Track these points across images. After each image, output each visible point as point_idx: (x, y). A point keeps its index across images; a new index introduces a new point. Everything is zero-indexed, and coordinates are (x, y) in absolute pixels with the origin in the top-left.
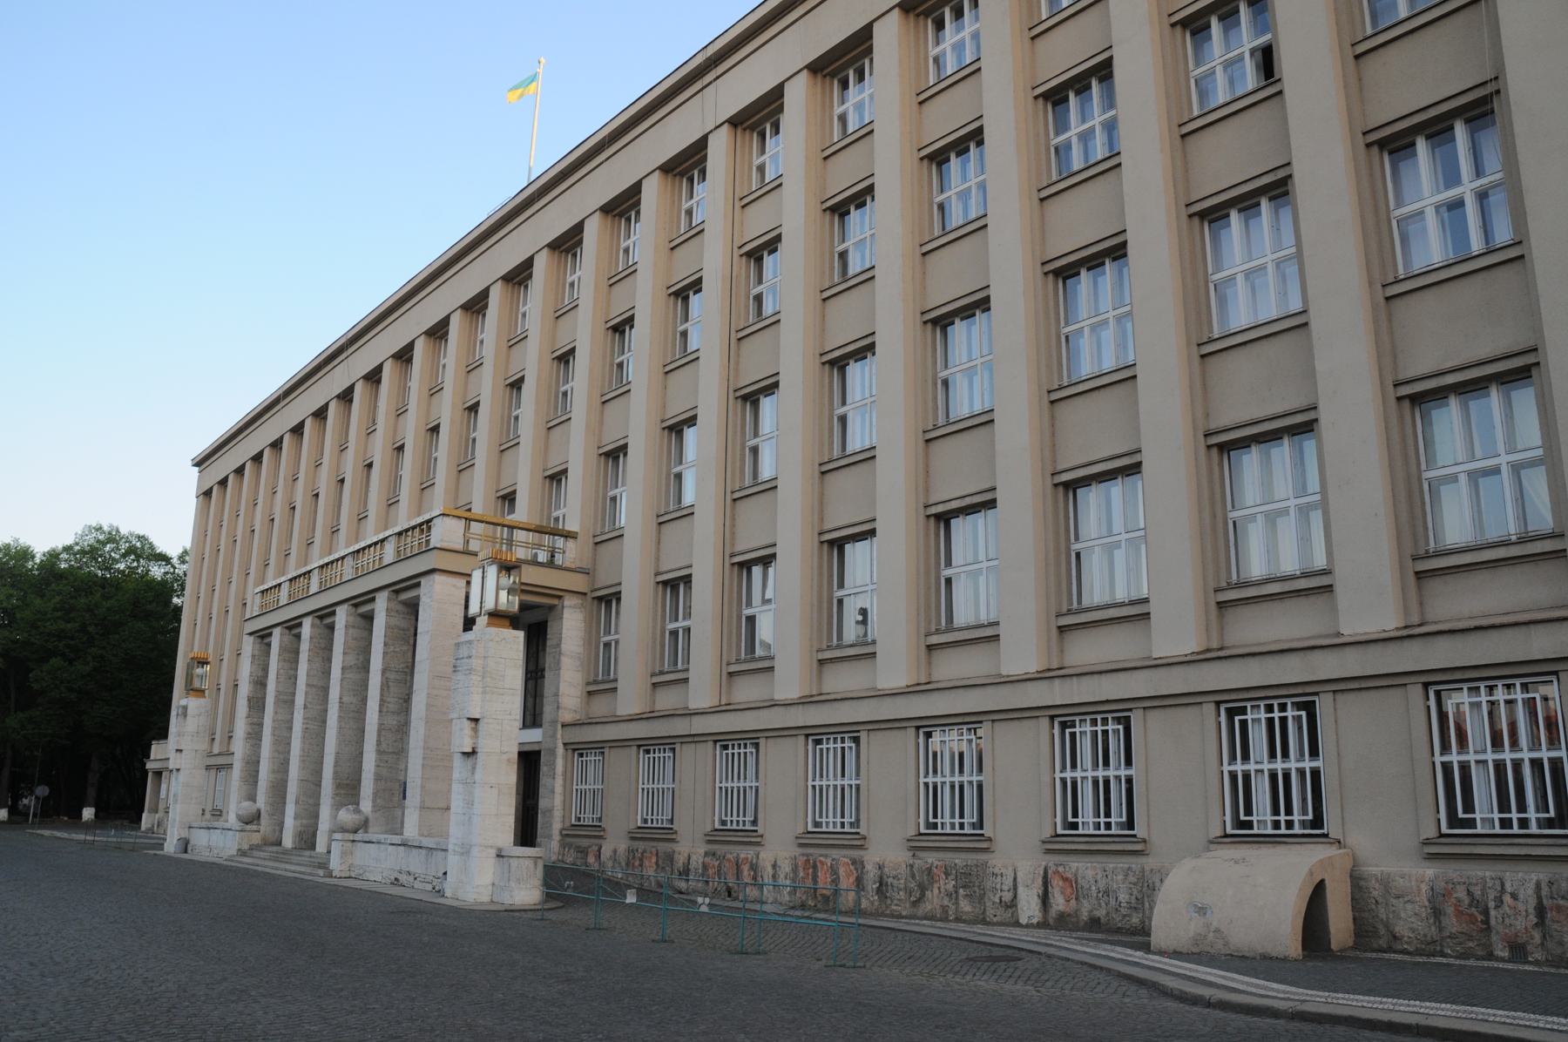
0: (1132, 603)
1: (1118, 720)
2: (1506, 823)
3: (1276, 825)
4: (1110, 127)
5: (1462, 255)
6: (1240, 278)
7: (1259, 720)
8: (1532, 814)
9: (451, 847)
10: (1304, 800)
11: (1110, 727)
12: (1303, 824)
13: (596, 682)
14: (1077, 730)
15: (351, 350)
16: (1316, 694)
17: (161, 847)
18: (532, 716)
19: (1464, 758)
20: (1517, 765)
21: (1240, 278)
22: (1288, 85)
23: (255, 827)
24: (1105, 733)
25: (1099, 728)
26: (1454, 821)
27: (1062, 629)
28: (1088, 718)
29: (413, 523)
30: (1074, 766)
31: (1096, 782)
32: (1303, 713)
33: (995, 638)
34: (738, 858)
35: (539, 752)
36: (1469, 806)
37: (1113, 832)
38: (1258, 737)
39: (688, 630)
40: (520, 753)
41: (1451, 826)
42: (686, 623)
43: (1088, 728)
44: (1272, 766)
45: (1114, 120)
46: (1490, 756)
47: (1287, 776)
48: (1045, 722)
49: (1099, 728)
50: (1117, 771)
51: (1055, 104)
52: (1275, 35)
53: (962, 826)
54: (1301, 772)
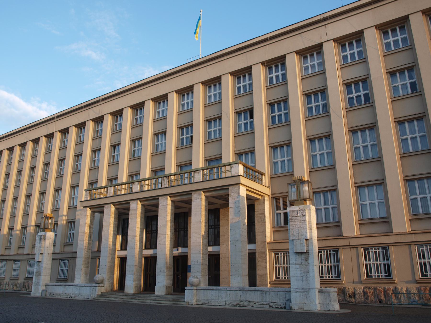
2: (378, 276)
3: (329, 277)
8: (334, 275)
9: (292, 290)
13: (7, 246)
15: (102, 102)
17: (30, 294)
18: (251, 239)
23: (102, 285)
27: (64, 245)
34: (385, 288)
38: (281, 260)
39: (73, 233)
40: (249, 253)
41: (422, 276)
42: (73, 232)
51: (181, 129)
52: (328, 101)
54: (335, 266)
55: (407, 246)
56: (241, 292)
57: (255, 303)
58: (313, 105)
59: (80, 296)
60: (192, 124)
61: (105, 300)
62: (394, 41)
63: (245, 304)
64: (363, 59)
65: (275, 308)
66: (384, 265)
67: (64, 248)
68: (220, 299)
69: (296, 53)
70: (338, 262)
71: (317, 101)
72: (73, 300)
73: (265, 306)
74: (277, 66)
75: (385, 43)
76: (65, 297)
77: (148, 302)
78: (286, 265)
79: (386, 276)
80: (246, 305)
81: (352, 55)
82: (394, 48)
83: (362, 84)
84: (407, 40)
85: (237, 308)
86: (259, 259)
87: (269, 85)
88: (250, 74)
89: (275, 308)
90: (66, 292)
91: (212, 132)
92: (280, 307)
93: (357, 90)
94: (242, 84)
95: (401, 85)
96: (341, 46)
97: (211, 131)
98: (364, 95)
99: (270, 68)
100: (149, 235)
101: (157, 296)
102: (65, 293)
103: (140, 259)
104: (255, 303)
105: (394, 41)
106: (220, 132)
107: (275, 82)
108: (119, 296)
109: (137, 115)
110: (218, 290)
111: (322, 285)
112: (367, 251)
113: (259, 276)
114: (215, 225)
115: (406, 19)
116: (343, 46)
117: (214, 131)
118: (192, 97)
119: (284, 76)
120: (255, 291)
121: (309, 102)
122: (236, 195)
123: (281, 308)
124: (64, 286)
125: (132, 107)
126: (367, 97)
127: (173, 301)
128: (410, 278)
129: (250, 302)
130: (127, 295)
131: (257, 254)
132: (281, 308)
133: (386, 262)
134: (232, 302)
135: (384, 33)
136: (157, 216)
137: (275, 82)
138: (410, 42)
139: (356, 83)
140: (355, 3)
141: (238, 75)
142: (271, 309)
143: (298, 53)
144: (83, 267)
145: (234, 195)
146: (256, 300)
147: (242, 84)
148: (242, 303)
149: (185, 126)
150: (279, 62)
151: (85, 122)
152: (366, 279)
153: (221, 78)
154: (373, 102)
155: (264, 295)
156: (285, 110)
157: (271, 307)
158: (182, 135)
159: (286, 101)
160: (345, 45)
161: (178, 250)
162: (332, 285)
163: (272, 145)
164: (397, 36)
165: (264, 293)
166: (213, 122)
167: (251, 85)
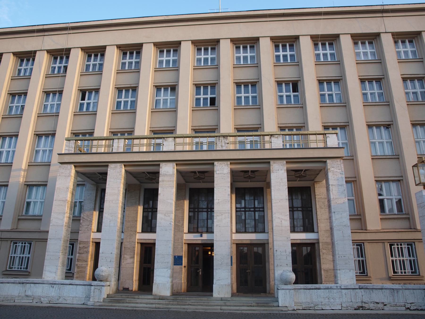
0: (38, 216)
1: (29, 243)
3: (402, 273)
4: (59, 105)
5: (6, 162)
6: (41, 151)
7: (406, 247)
11: (26, 245)
12: (24, 268)
14: (18, 245)
15: (71, 32)
20: (396, 261)
21: (41, 151)
24: (25, 246)
25: (23, 245)
28: (21, 242)
30: (15, 253)
31: (20, 257)
33: (41, 219)
37: (22, 270)
43: (20, 244)
45: (60, 104)
46: (409, 258)
48: (9, 242)
49: (23, 245)
50: (26, 255)
51: (47, 94)
55: (381, 243)
56: (362, 290)
57: (385, 305)
58: (123, 100)
59: (60, 301)
60: (63, 91)
61: (127, 306)
62: (204, 59)
63: (372, 306)
64: (176, 68)
65: (414, 310)
66: (400, 261)
67: (18, 224)
68: (332, 300)
69: (117, 47)
70: (362, 256)
71: (205, 93)
72: (45, 307)
73: (399, 308)
74: (96, 56)
75: (197, 59)
76: (26, 302)
77: (200, 308)
78: (412, 258)
79: (361, 273)
80: (373, 308)
81: (168, 62)
82: (173, 66)
83: (203, 89)
84: (208, 61)
85: (360, 312)
86: (324, 251)
87: (120, 69)
88: (103, 55)
89: (414, 310)
90: (27, 294)
91: (14, 107)
92: (420, 308)
93: (126, 97)
94: (58, 65)
95: (170, 99)
96: (123, 54)
97: (48, 105)
98: (211, 98)
99: (90, 56)
100: (192, 214)
101: (217, 299)
102: (27, 296)
103: (228, 244)
104: (385, 305)
105: (166, 60)
106: (58, 107)
107: (127, 68)
108: (148, 301)
109: (21, 65)
110: (328, 289)
111: (358, 282)
112: (393, 247)
113: (324, 270)
114: (207, 208)
115: (217, 41)
116: (125, 54)
117: (16, 106)
118: (33, 65)
119: (138, 64)
120: (382, 289)
121: (120, 96)
122: (338, 171)
123: (422, 310)
124: (23, 283)
125: (120, 47)
126: (213, 101)
127: (258, 306)
128: (384, 276)
129: (378, 303)
130: (162, 298)
131: (321, 244)
132: (422, 310)
133: (361, 259)
134: (351, 304)
135: (236, 47)
136: (213, 189)
137: (127, 68)
138: (217, 63)
139: (206, 86)
140: (263, 11)
141: (131, 49)
142: (408, 312)
143: (156, 45)
144: (61, 254)
145: (335, 170)
146: (386, 301)
147: (58, 65)
148: (366, 305)
149: (88, 90)
150: (135, 50)
151: (35, 52)
152: (393, 275)
153: (106, 48)
154: (219, 106)
155: (396, 295)
156: (88, 100)
157: (408, 308)
158: (281, 91)
159: (135, 89)
160: (126, 53)
161: (201, 236)
162: (413, 282)
163: (194, 128)
164: (208, 55)
165: (396, 291)
166: (51, 95)
167: (101, 65)
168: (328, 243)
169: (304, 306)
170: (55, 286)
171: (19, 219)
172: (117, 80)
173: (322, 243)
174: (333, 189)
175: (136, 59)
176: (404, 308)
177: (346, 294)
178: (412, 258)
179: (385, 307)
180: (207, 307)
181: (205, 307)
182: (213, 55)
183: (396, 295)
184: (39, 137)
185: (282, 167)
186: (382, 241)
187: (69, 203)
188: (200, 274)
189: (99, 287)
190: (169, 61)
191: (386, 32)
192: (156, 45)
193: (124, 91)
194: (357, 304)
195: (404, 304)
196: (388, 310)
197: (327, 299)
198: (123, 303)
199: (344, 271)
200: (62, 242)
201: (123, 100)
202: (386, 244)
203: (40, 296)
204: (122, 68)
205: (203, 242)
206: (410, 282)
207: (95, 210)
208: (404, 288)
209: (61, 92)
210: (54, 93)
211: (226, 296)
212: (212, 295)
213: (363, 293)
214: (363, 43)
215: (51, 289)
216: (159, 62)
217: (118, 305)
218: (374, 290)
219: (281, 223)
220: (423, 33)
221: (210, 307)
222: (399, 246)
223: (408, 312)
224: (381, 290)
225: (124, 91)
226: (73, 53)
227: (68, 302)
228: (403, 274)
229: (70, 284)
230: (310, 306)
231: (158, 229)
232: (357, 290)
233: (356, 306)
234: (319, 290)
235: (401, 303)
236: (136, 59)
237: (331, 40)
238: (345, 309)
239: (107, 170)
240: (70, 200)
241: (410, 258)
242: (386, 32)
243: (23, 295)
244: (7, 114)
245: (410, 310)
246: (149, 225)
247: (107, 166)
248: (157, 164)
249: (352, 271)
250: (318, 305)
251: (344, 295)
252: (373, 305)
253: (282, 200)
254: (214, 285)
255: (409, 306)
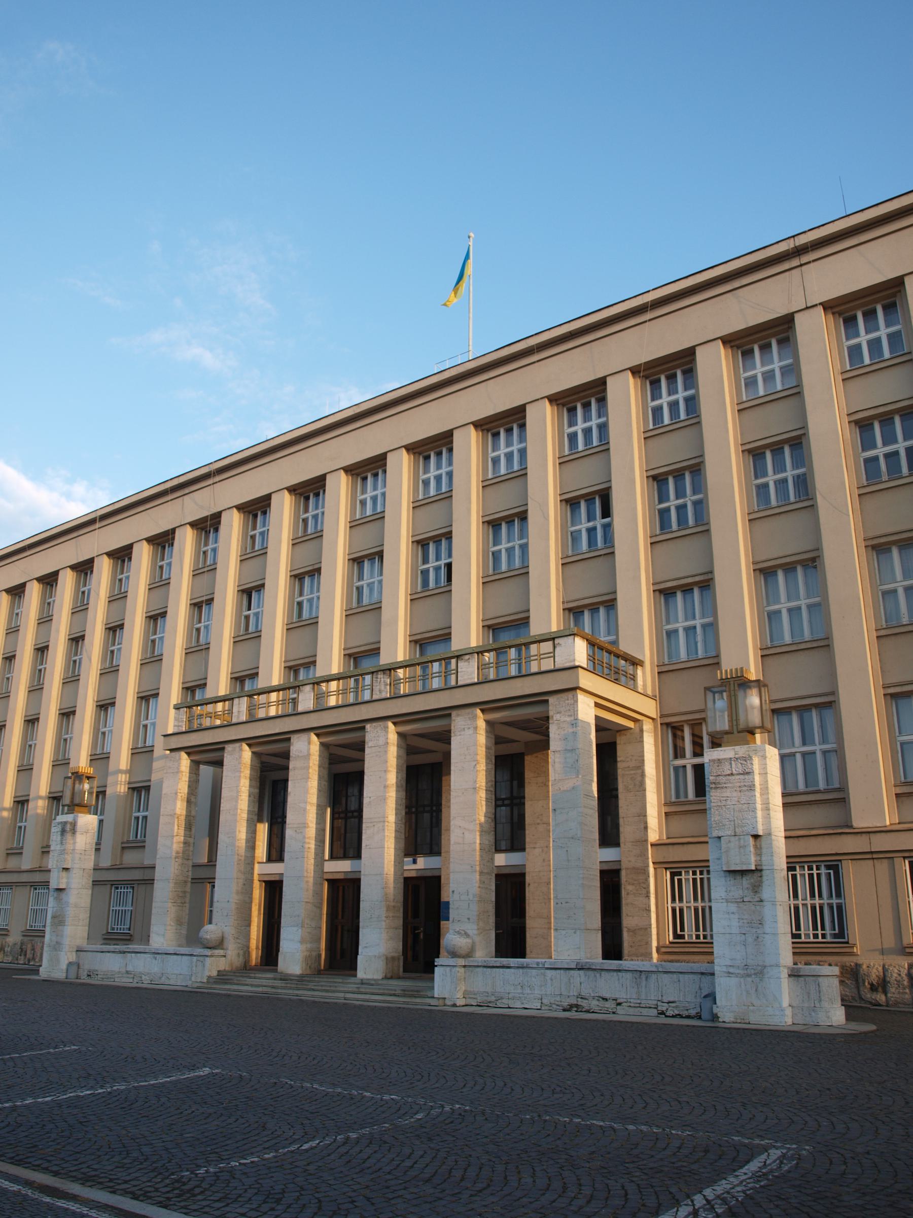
3: (816, 936)
8: (828, 931)
10: (833, 921)
15: (217, 479)
16: (840, 861)
19: (681, 905)
22: (612, 446)
26: (676, 936)
29: (514, 643)
32: (831, 872)
35: (281, 882)
36: (682, 929)
39: (145, 818)
42: (145, 814)
44: (681, 905)
46: (809, 902)
47: (821, 908)
48: (109, 886)
53: (824, 936)
54: (831, 907)
55: (886, 861)
56: (581, 972)
57: (619, 1004)
58: (771, 479)
59: (163, 980)
62: (870, 343)
63: (594, 1004)
65: (673, 1016)
67: (122, 856)
68: (528, 991)
69: (724, 343)
70: (839, 895)
71: (780, 467)
73: (645, 1012)
74: (672, 378)
75: (745, 379)
76: (125, 981)
80: (596, 1009)
81: (875, 345)
82: (891, 353)
85: (573, 1014)
86: (630, 888)
89: (673, 1016)
92: (685, 1013)
102: (127, 972)
104: (619, 1004)
110: (523, 967)
113: (629, 930)
116: (850, 322)
119: (692, 403)
120: (619, 971)
121: (760, 471)
122: (568, 719)
123: (688, 1017)
125: (295, 490)
129: (606, 1000)
132: (688, 1017)
134: (558, 998)
137: (667, 420)
141: (570, 402)
142: (662, 1020)
144: (170, 905)
145: (563, 719)
146: (622, 996)
148: (584, 1003)
151: (173, 531)
155: (644, 983)
157: (662, 1013)
158: (425, 560)
161: (415, 862)
162: (824, 958)
165: (643, 976)
167: (603, 428)
168: (638, 869)
169: (480, 999)
170: (158, 956)
171: (123, 848)
172: (562, 481)
173: (627, 869)
174: (557, 760)
175: (686, 389)
176: (655, 1011)
177: (552, 980)
178: (700, 904)
179: (619, 1007)
180: (327, 994)
181: (324, 994)
182: (690, 389)
183: (644, 983)
184: (493, 630)
185: (469, 722)
186: (888, 855)
187: (183, 818)
188: (422, 936)
189: (201, 959)
190: (878, 340)
191: (807, 308)
192: (729, 341)
193: (768, 455)
194: (568, 1000)
195: (655, 1002)
196: (623, 1014)
197: (519, 987)
198: (231, 984)
199: (564, 932)
200: (172, 885)
201: (673, 503)
202: (898, 861)
203: (140, 973)
204: (654, 424)
205: (420, 874)
206: (809, 958)
207: (260, 820)
208: (660, 970)
209: (523, 516)
210: (509, 520)
211: (375, 977)
212: (355, 976)
213: (583, 979)
214: (765, 348)
215: (154, 961)
216: (746, 385)
217: (221, 986)
218: (603, 973)
219: (463, 838)
220: (907, 281)
221: (330, 994)
222: (815, 872)
223: (662, 1020)
224: (615, 974)
225: (768, 455)
226: (613, 388)
227: (172, 982)
228: (820, 939)
229: (175, 954)
230: (489, 999)
231: (287, 856)
232: (572, 972)
233: (565, 1004)
234: (508, 970)
235: (650, 1002)
236: (686, 389)
237: (599, 393)
238: (547, 1008)
239: (223, 756)
240: (184, 813)
241: (796, 902)
242: (807, 308)
243: (124, 970)
244: (108, 665)
245: (666, 1016)
246: (276, 852)
247: (223, 749)
248: (285, 738)
249: (578, 932)
250: (502, 998)
251: (549, 981)
252: (597, 1003)
253: (466, 790)
254: (359, 957)
255: (664, 1009)
